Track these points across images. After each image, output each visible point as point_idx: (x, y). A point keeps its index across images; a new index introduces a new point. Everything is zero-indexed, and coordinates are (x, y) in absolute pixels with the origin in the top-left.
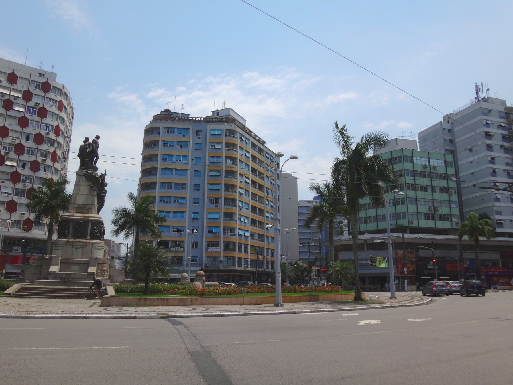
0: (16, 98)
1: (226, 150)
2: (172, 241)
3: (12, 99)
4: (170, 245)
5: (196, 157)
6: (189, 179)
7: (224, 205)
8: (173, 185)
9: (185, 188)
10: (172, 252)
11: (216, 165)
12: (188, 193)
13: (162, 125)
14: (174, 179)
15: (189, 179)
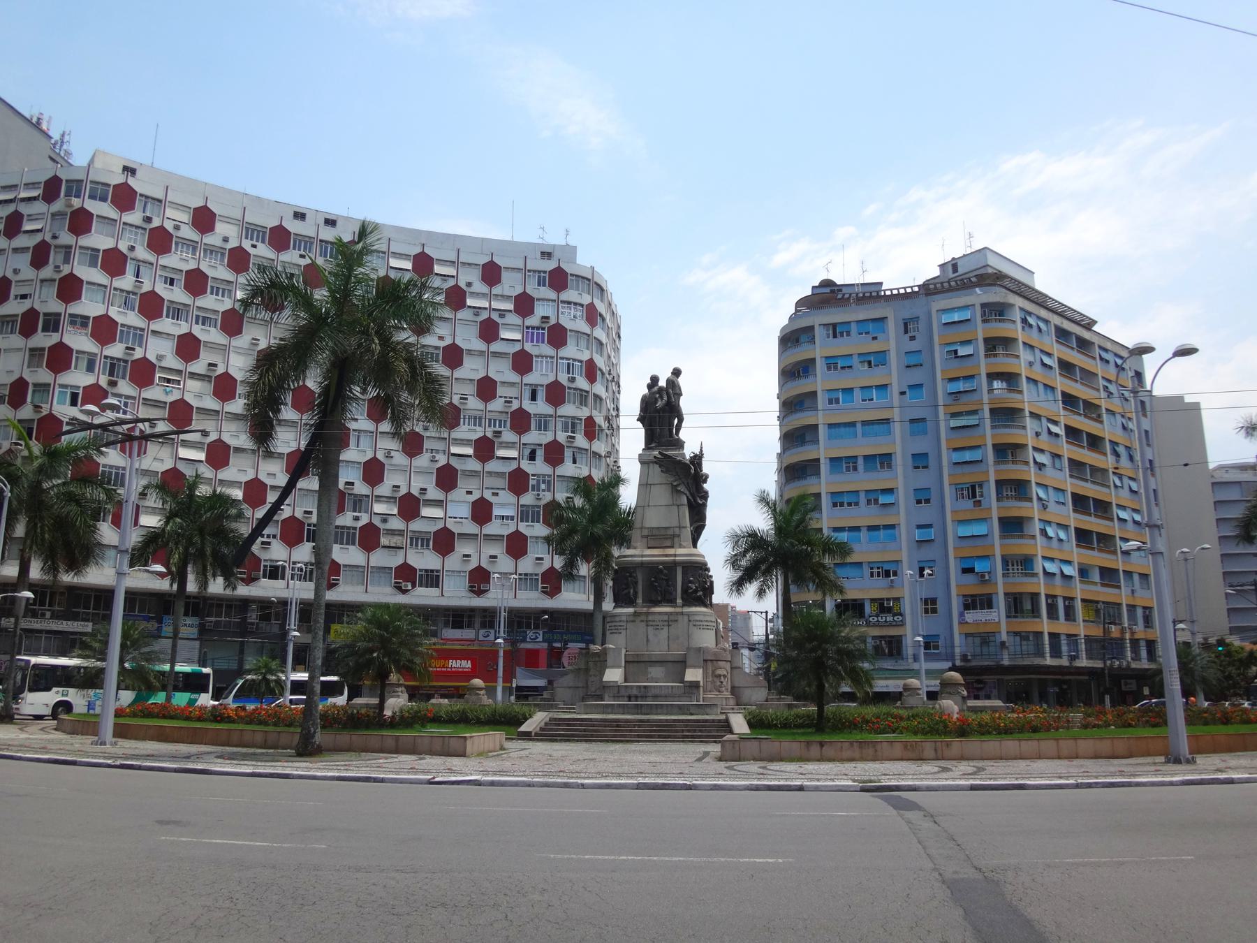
0: (502, 313)
1: (986, 356)
2: (873, 600)
3: (495, 316)
4: (868, 609)
5: (910, 387)
6: (898, 443)
7: (998, 500)
8: (860, 461)
9: (890, 466)
10: (874, 626)
11: (964, 398)
12: (901, 478)
13: (819, 319)
14: (862, 446)
15: (898, 443)
